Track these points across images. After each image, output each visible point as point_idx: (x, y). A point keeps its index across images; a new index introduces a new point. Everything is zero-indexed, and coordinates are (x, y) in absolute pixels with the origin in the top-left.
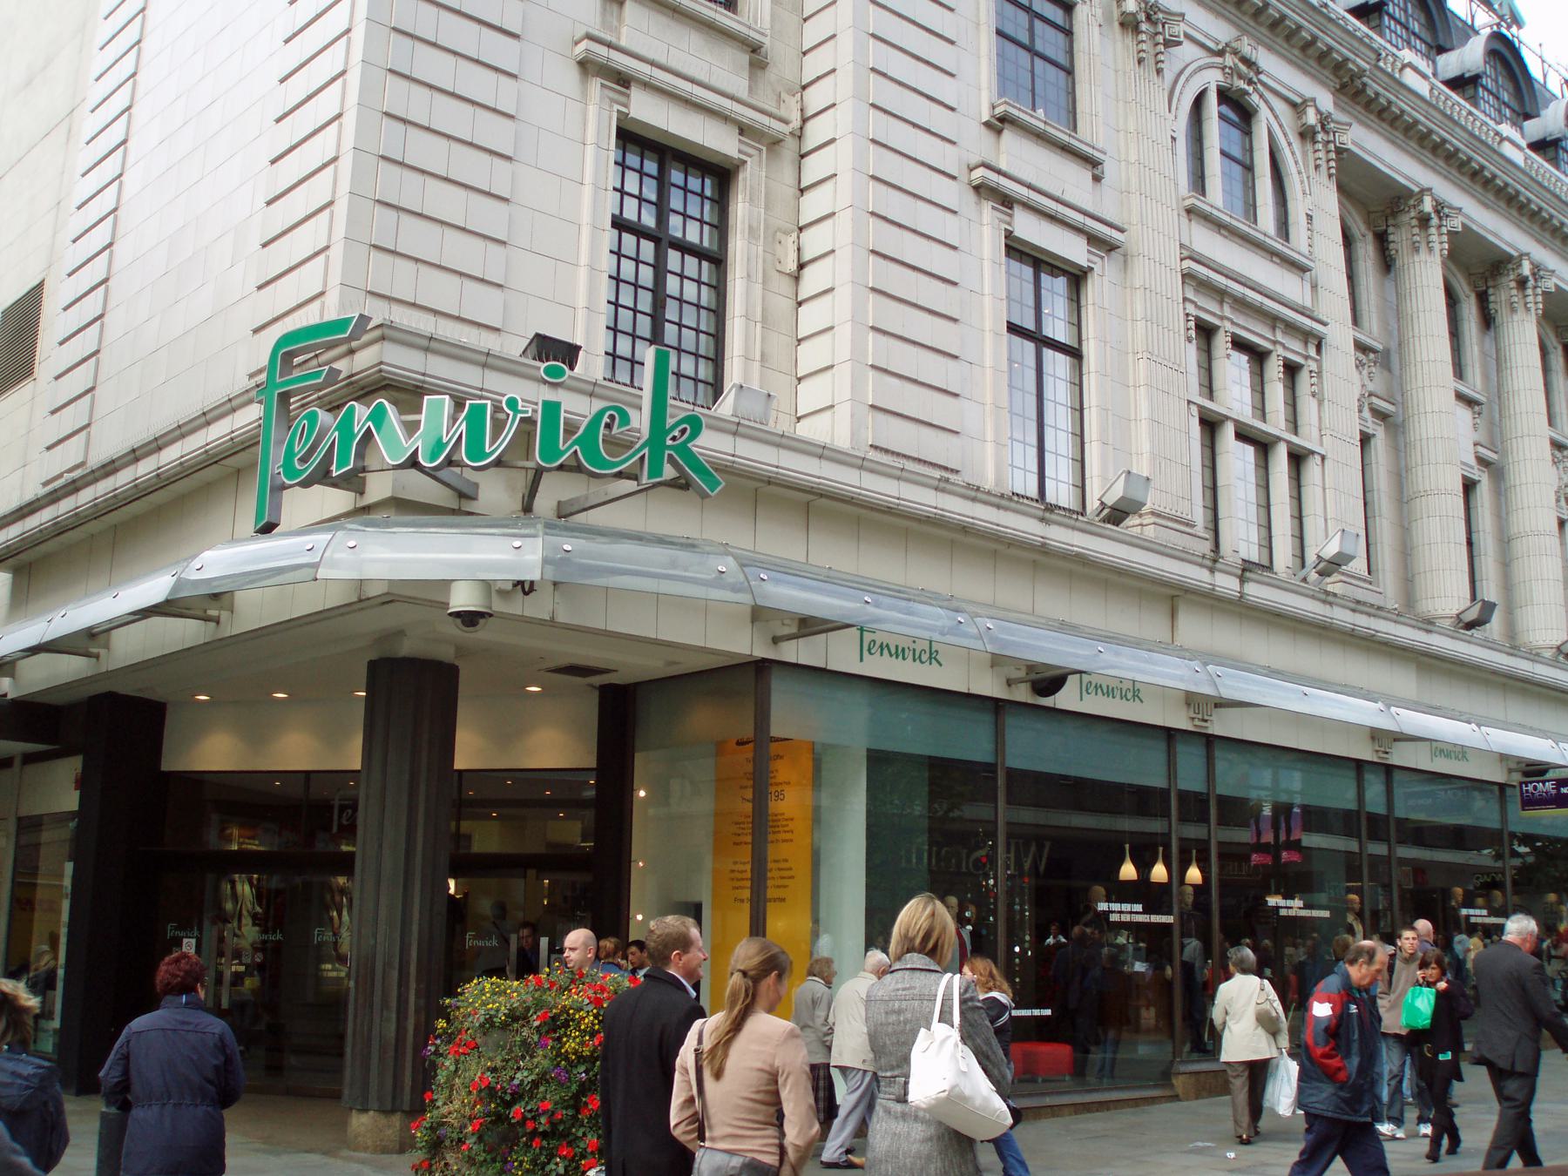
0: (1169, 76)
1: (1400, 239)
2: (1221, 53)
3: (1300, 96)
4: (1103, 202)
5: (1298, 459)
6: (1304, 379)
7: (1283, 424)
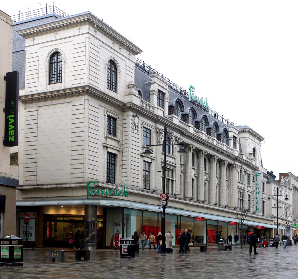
1: (222, 164)
5: (172, 181)
7: (171, 155)
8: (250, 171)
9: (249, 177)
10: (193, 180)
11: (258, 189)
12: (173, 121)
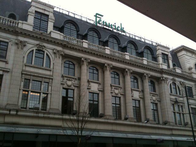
0: (167, 83)
2: (37, 45)
5: (183, 114)
6: (183, 107)
12: (51, 35)
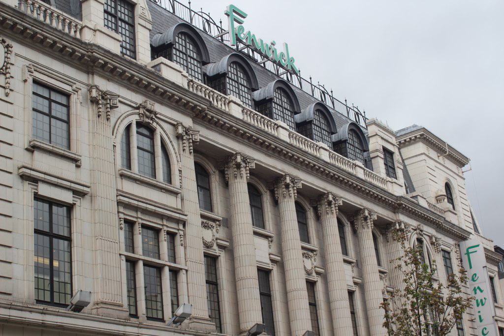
0: (113, 120)
1: (230, 172)
2: (138, 108)
3: (176, 121)
4: (82, 176)
5: (175, 272)
6: (178, 239)
8: (447, 242)
9: (448, 261)
10: (351, 293)
11: (478, 291)
